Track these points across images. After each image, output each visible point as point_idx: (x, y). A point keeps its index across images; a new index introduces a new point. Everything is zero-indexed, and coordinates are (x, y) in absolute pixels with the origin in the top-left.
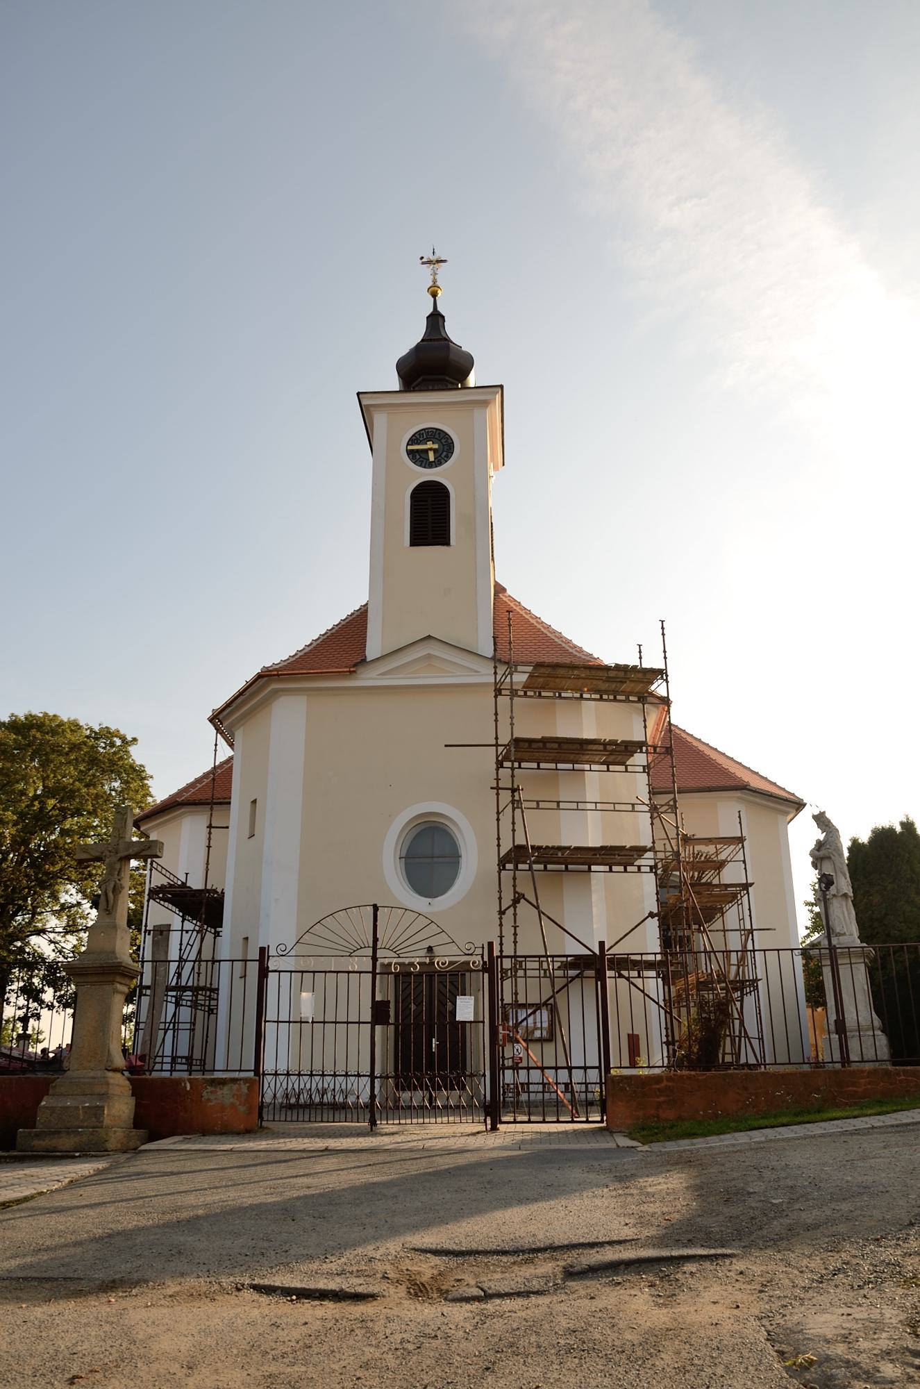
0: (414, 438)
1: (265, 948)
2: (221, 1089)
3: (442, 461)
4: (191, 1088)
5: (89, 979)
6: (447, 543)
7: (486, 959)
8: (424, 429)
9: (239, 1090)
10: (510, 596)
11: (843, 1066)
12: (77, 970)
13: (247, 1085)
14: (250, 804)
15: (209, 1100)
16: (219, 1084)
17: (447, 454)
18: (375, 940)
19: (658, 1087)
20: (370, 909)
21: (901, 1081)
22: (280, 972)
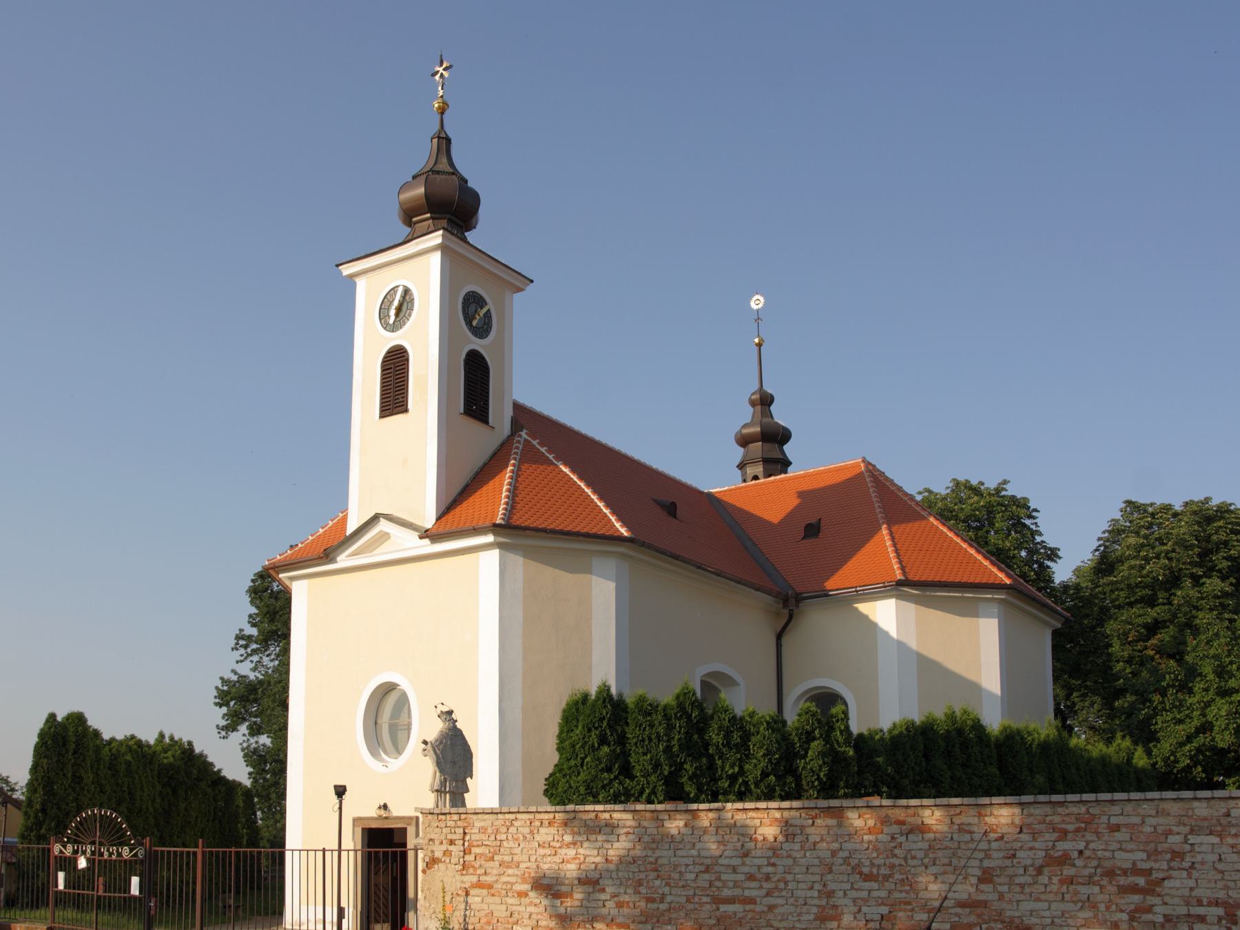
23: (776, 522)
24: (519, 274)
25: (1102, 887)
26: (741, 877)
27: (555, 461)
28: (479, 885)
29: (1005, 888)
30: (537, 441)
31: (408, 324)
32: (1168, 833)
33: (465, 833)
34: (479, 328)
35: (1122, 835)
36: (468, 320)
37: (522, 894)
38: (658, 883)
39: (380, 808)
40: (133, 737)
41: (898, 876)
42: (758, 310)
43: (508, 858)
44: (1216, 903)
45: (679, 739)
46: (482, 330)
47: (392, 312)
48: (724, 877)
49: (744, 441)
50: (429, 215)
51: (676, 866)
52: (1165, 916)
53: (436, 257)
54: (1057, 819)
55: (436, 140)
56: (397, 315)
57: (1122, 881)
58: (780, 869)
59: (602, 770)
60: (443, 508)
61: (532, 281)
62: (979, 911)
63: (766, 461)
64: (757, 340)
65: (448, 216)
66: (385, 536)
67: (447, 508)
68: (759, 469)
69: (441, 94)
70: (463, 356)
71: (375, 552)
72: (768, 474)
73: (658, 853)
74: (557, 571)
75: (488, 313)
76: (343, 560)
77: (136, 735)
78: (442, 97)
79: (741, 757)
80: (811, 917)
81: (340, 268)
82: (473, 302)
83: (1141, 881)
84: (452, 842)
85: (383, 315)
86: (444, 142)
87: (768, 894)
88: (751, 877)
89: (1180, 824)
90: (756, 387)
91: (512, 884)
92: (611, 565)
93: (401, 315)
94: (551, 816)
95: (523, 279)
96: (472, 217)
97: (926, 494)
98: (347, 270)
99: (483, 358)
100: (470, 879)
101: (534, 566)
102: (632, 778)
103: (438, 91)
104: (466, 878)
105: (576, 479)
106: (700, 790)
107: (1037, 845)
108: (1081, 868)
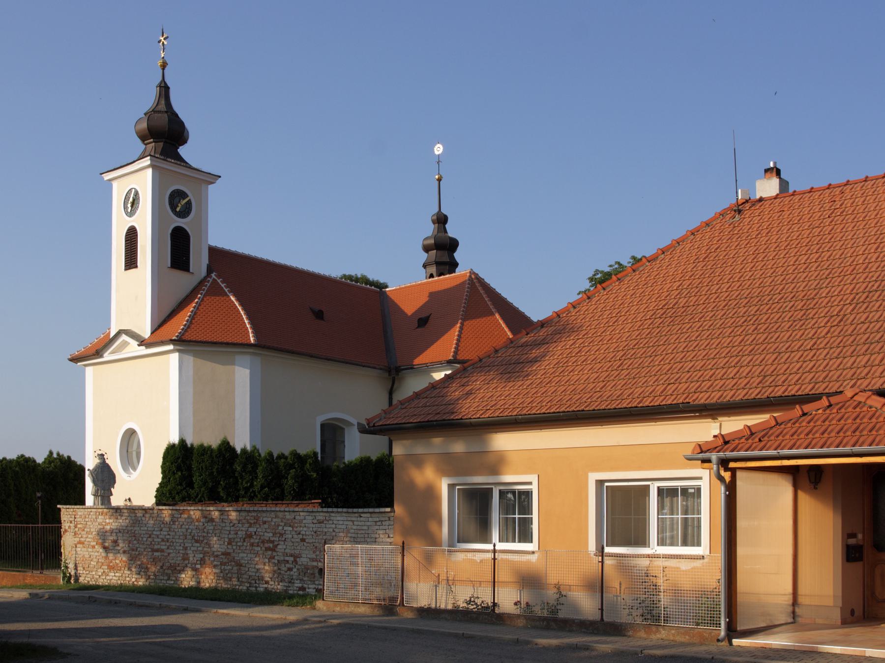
23: (409, 315)
24: (210, 174)
25: (261, 548)
26: (160, 540)
27: (228, 293)
28: (80, 542)
29: (234, 547)
30: (221, 279)
31: (138, 212)
32: (279, 525)
33: (75, 518)
34: (182, 212)
35: (266, 526)
36: (173, 207)
37: (93, 547)
38: (135, 542)
39: (126, 500)
40: (22, 456)
41: (205, 541)
42: (439, 155)
43: (88, 530)
44: (291, 555)
45: (217, 469)
46: (185, 212)
47: (129, 205)
48: (155, 540)
49: (427, 249)
50: (152, 140)
51: (141, 534)
52: (278, 560)
53: (150, 171)
54: (249, 518)
55: (158, 88)
56: (132, 206)
57: (266, 545)
58: (171, 537)
59: (177, 485)
60: (156, 326)
61: (220, 177)
62: (228, 557)
63: (438, 264)
64: (437, 177)
65: (164, 140)
66: (126, 344)
67: (158, 326)
68: (433, 269)
69: (163, 56)
70: (170, 231)
71: (123, 352)
72: (440, 275)
73: (135, 528)
74: (214, 364)
75: (189, 203)
76: (107, 356)
77: (25, 454)
78: (163, 58)
79: (252, 478)
80: (180, 558)
81: (103, 175)
82: (176, 197)
83: (271, 545)
84: (71, 522)
85: (125, 208)
86: (164, 90)
87: (168, 548)
88: (163, 540)
89: (282, 521)
90: (437, 210)
91: (90, 542)
92: (247, 359)
93: (135, 206)
94: (102, 510)
95: (213, 177)
96: (184, 132)
97: (617, 266)
98: (107, 177)
99: (185, 231)
100: (77, 540)
101: (199, 361)
102: (193, 488)
103: (161, 54)
104: (76, 539)
105: (237, 305)
106: (228, 495)
107: (243, 529)
108: (255, 540)
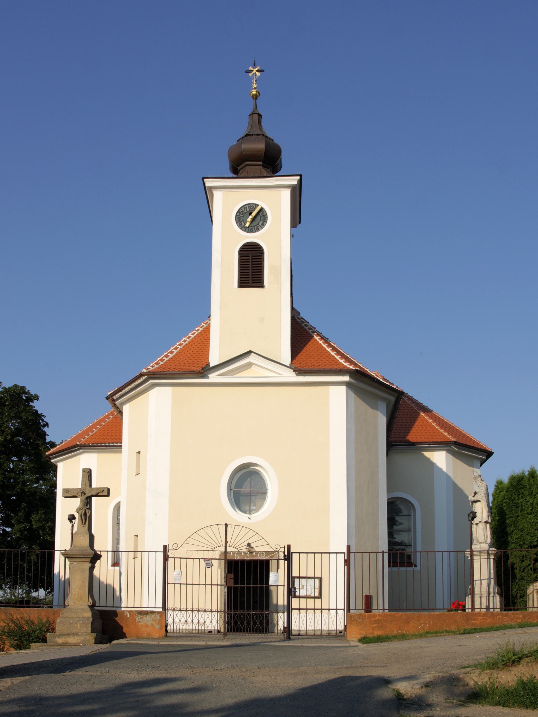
0: (241, 210)
1: (166, 546)
2: (145, 616)
3: (260, 228)
4: (130, 616)
5: (76, 560)
6: (262, 286)
7: (286, 554)
8: (248, 204)
9: (155, 617)
10: (302, 318)
11: (472, 611)
12: (70, 555)
13: (160, 615)
14: (135, 453)
15: (139, 622)
16: (144, 614)
17: (263, 223)
18: (226, 542)
19: (373, 619)
20: (224, 526)
21: (499, 619)
22: (175, 558)
66: (250, 365)
98: (209, 183)
